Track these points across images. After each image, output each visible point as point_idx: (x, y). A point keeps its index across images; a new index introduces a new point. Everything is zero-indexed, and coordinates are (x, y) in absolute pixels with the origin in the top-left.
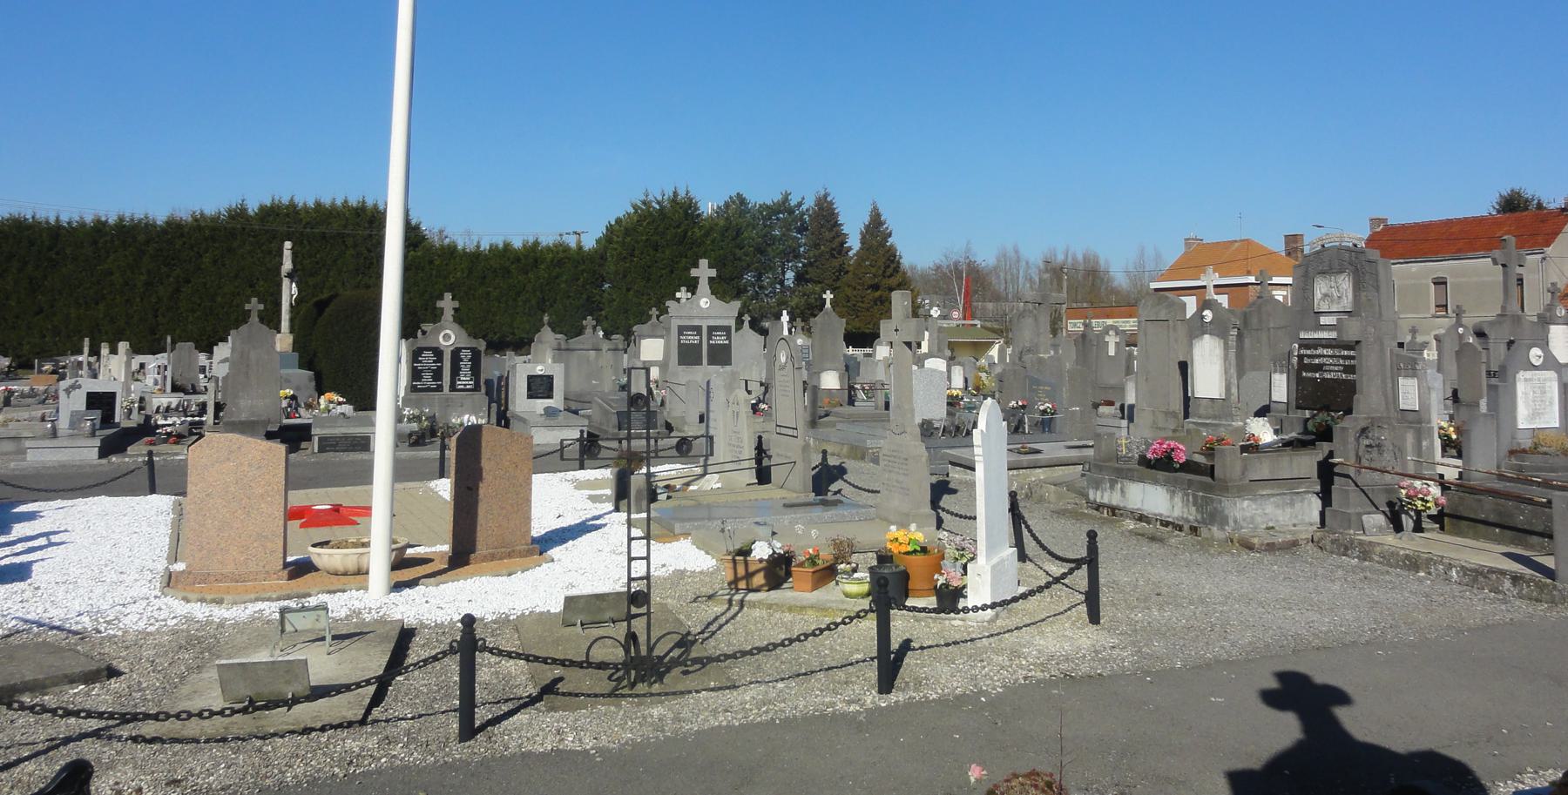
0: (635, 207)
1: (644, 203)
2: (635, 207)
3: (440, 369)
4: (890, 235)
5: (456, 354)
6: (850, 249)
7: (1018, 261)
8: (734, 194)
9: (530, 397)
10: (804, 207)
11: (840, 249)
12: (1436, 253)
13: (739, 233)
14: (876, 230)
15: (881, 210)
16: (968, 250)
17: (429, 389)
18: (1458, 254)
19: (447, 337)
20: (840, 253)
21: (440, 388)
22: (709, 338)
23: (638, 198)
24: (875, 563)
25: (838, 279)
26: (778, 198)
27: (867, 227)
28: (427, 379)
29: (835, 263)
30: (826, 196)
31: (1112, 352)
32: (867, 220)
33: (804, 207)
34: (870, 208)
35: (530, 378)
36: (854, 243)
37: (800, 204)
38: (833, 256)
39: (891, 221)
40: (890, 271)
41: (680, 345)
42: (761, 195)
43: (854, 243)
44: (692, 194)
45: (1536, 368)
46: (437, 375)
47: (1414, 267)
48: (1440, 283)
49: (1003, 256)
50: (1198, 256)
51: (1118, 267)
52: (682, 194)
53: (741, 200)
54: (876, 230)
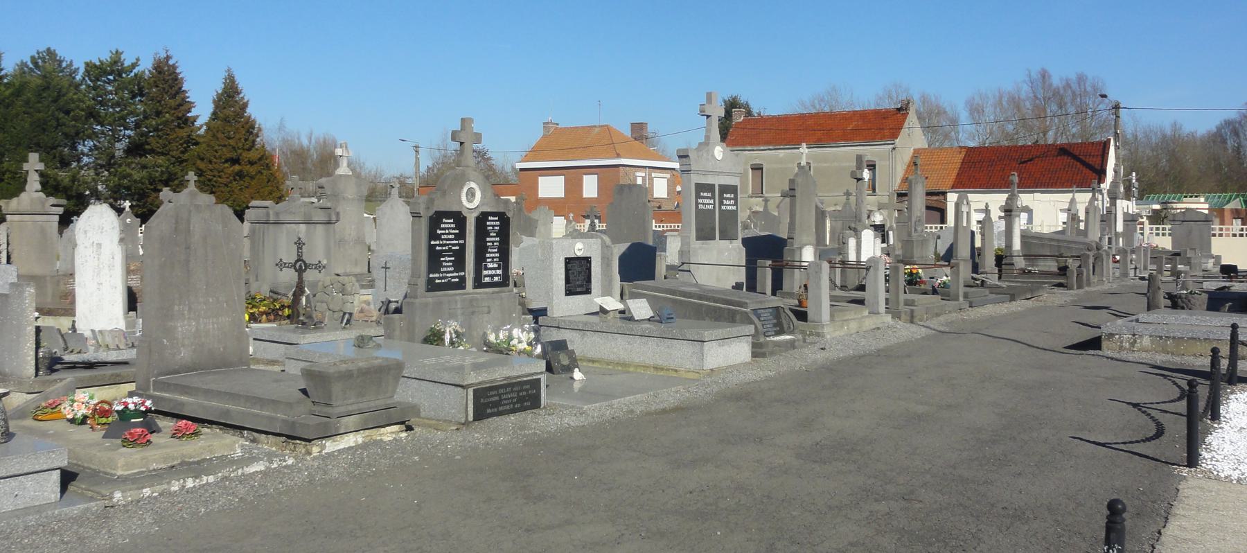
3: (463, 247)
5: (482, 219)
6: (195, 119)
8: (42, 48)
9: (569, 292)
12: (874, 139)
13: (60, 95)
14: (230, 101)
17: (450, 286)
19: (471, 194)
21: (461, 284)
22: (721, 204)
24: (15, 280)
26: (106, 57)
28: (448, 270)
29: (183, 133)
30: (168, 58)
32: (219, 87)
34: (224, 75)
35: (568, 261)
36: (202, 111)
37: (134, 66)
38: (179, 126)
41: (698, 211)
42: (80, 52)
43: (202, 111)
45: (493, 214)
46: (459, 264)
47: (782, 153)
48: (758, 168)
50: (556, 141)
54: (230, 101)
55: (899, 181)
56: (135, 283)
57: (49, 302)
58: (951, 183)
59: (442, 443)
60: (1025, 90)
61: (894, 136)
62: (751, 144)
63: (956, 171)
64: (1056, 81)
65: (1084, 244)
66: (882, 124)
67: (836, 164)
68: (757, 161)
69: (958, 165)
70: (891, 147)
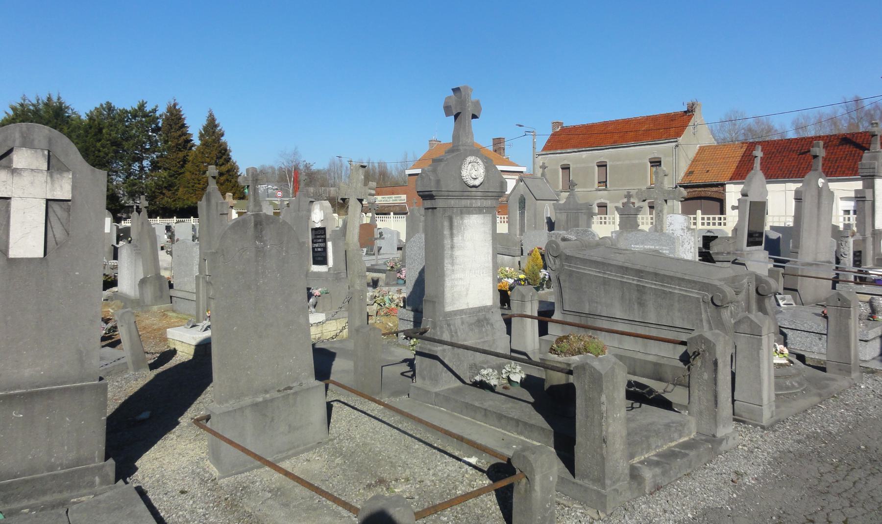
0: (14, 109)
1: (22, 105)
2: (14, 109)
4: (222, 135)
7: (341, 166)
10: (158, 114)
11: (187, 142)
12: (660, 138)
14: (211, 129)
15: (216, 117)
16: (295, 153)
18: (615, 144)
20: (185, 147)
23: (16, 101)
25: (183, 166)
27: (205, 129)
30: (175, 105)
31: (26, 240)
32: (205, 123)
33: (158, 114)
34: (207, 114)
36: (196, 141)
39: (223, 124)
40: (221, 161)
42: (125, 102)
44: (62, 100)
47: (584, 155)
48: (602, 165)
49: (333, 163)
51: (392, 168)
52: (55, 99)
53: (110, 108)
54: (211, 129)
55: (682, 174)
56: (113, 262)
57: (714, 248)
58: (730, 175)
59: (380, 452)
60: (841, 111)
61: (679, 134)
62: (562, 148)
63: (735, 165)
64: (867, 105)
65: (704, 287)
66: (670, 126)
67: (627, 162)
68: (566, 162)
69: (739, 159)
70: (674, 144)
